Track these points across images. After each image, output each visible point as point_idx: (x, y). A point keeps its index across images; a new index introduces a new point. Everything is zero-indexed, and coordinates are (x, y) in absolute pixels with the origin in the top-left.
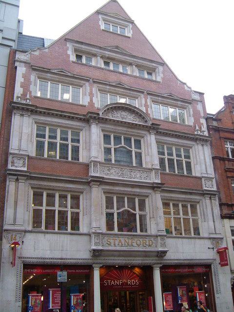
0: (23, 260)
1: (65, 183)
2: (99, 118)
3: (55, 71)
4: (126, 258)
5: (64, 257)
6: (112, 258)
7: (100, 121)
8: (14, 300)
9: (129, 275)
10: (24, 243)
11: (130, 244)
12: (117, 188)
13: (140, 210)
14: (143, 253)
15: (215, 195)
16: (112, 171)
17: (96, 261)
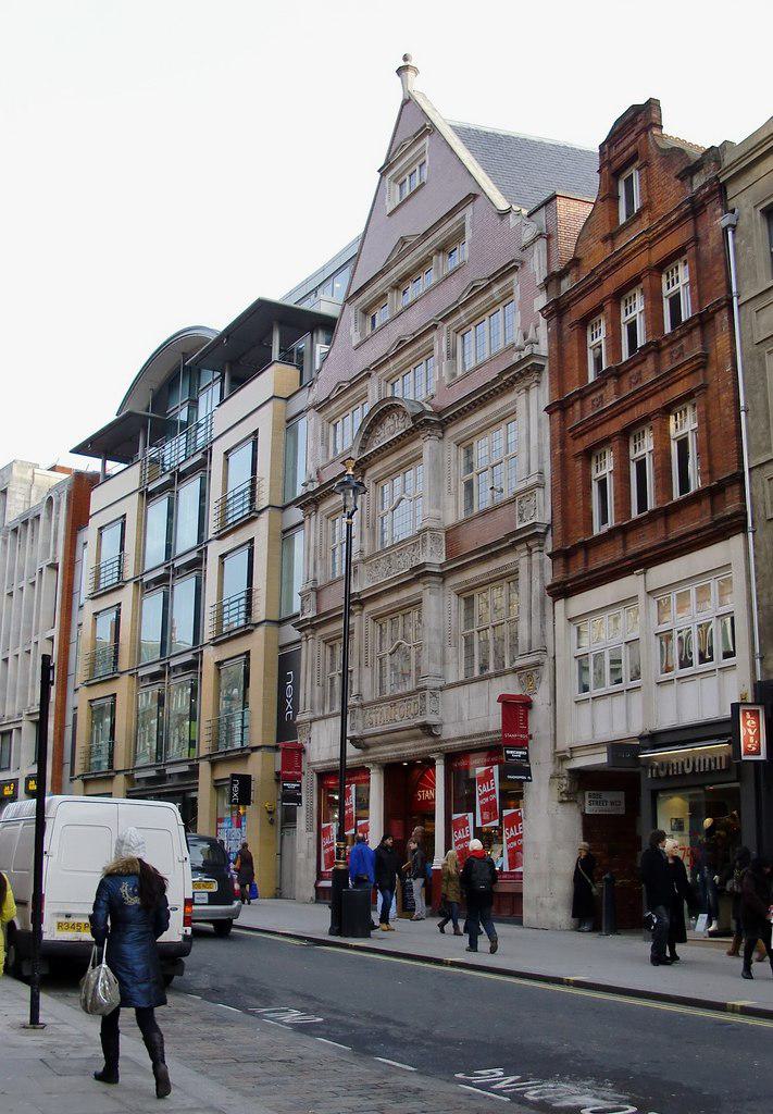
7: (364, 466)
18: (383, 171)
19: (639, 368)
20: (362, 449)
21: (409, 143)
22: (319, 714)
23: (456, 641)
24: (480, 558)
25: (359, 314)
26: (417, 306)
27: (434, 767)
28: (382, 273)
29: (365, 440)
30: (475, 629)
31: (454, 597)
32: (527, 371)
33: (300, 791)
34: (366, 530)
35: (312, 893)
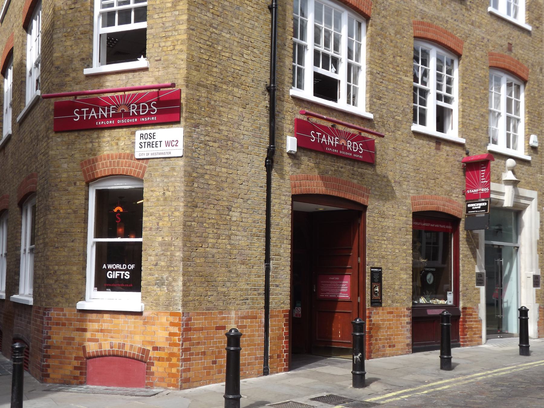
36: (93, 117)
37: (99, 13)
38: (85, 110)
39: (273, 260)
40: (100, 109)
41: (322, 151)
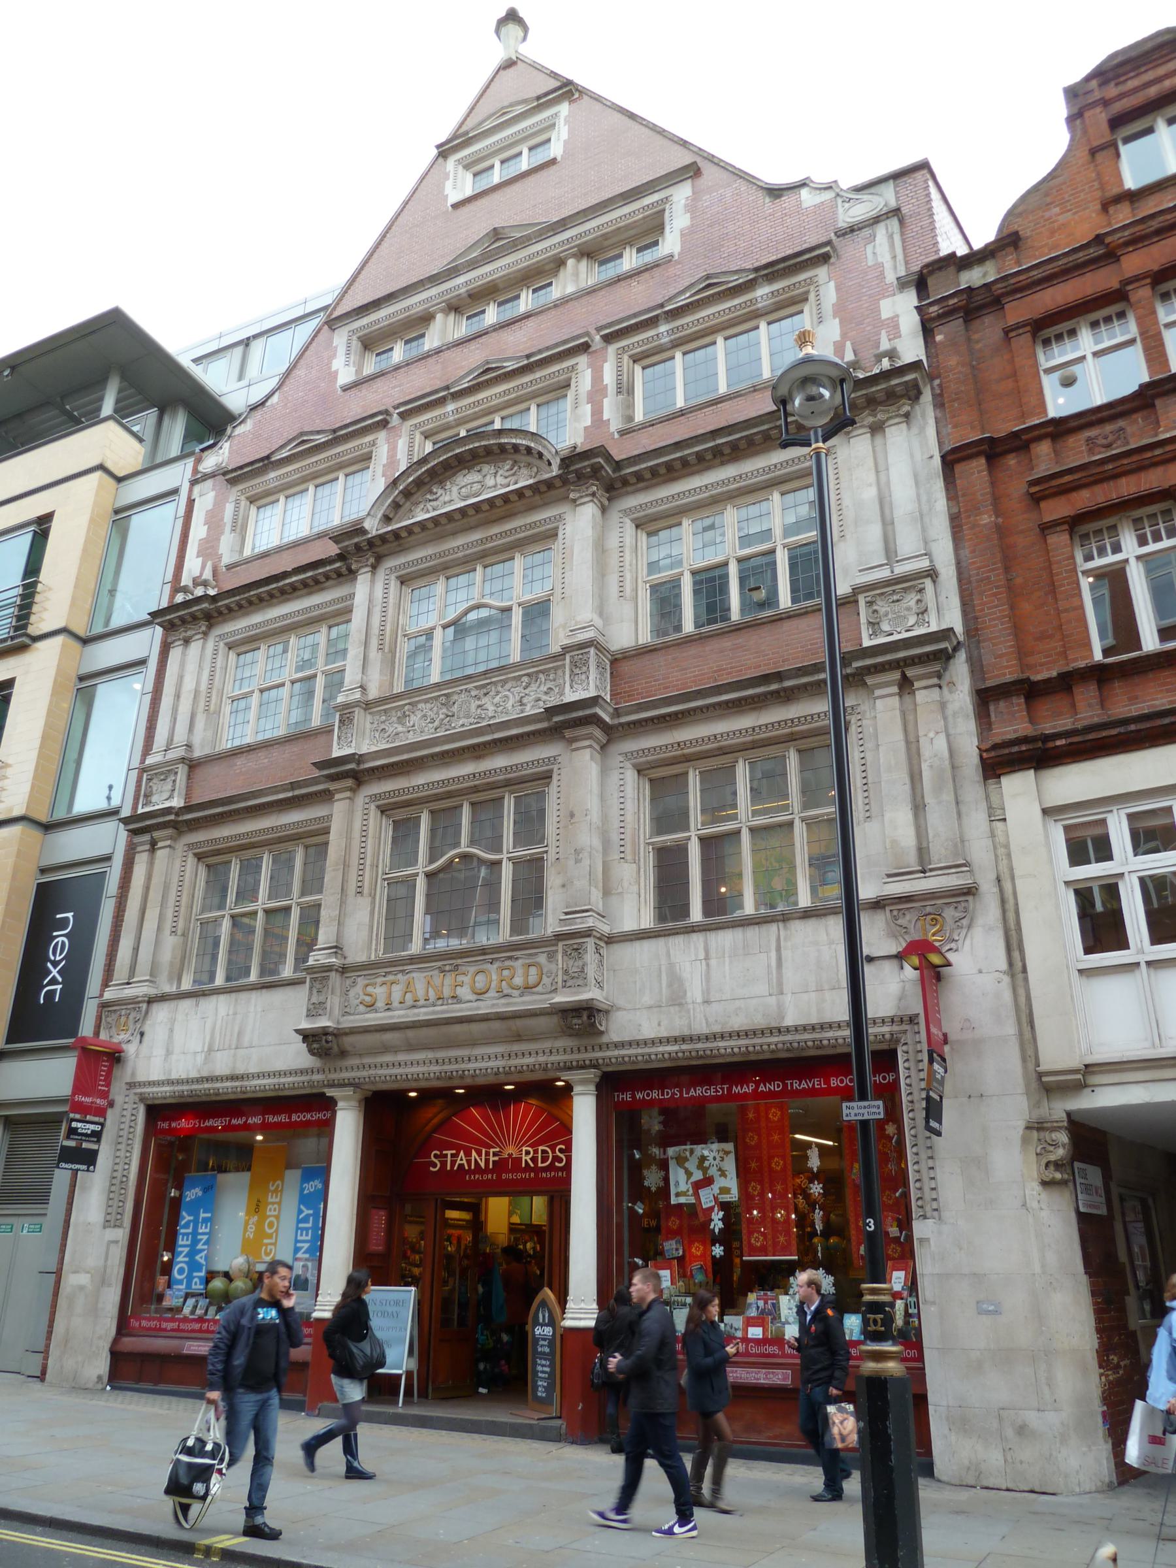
0: (139, 1091)
1: (280, 811)
2: (371, 543)
3: (284, 453)
4: (441, 1054)
5: (241, 1069)
6: (388, 1058)
7: (381, 550)
8: (102, 1220)
9: (523, 1121)
10: (146, 1038)
11: (447, 992)
12: (421, 779)
13: (521, 838)
14: (496, 1025)
15: (945, 657)
16: (415, 719)
17: (334, 1076)
18: (444, 151)
19: (1121, 423)
20: (387, 519)
21: (520, 109)
22: (169, 988)
23: (636, 852)
24: (739, 700)
25: (356, 345)
26: (531, 323)
27: (327, 1127)
28: (434, 280)
29: (396, 506)
30: (226, 913)
31: (631, 775)
32: (194, 618)
33: (98, 1141)
34: (374, 654)
35: (102, 1366)
36: (461, 1166)
37: (1061, 110)
38: (449, 1153)
39: (170, 1071)
40: (474, 1153)
41: (558, 84)
